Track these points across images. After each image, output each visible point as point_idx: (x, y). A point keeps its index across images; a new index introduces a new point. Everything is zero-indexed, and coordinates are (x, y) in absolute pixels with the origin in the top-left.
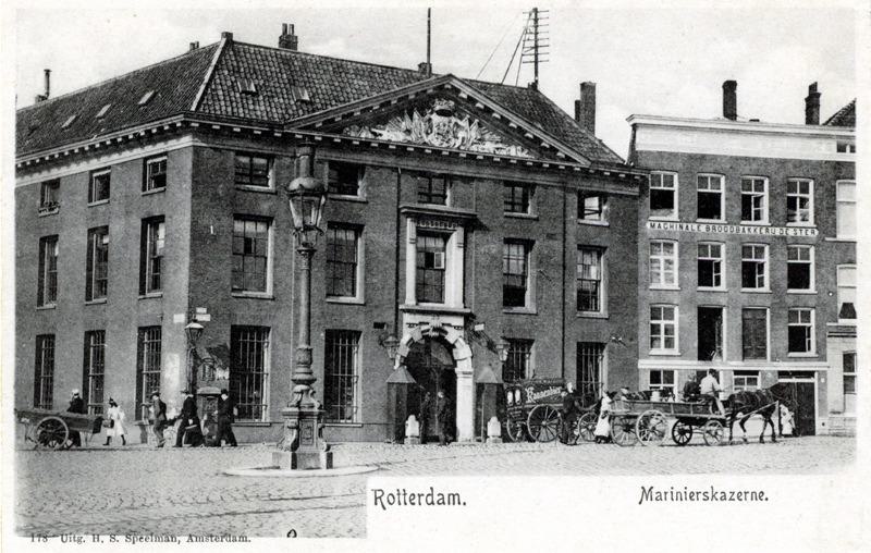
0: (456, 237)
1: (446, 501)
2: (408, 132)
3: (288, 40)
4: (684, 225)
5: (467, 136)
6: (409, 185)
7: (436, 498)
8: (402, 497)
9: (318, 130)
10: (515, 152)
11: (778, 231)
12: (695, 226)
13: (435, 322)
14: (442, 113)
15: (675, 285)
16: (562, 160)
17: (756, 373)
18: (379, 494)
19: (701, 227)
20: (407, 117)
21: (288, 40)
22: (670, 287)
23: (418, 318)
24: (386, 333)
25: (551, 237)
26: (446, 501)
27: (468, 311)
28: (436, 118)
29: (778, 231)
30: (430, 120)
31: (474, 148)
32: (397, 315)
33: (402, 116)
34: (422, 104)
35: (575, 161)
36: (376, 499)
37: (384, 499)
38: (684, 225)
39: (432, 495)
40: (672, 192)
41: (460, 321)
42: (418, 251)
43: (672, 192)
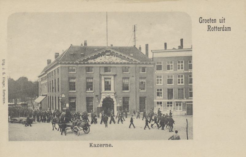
0: (113, 78)
1: (227, 30)
2: (101, 59)
3: (85, 44)
4: (164, 72)
5: (114, 59)
6: (103, 70)
7: (225, 29)
8: (215, 29)
9: (82, 61)
10: (124, 61)
11: (186, 72)
12: (166, 72)
13: (108, 95)
14: (107, 55)
15: (162, 84)
16: (134, 61)
17: (181, 102)
18: (209, 27)
19: (168, 72)
20: (101, 57)
21: (85, 44)
22: (161, 85)
23: (105, 94)
24: (98, 97)
25: (133, 77)
26: (227, 30)
27: (115, 92)
28: (107, 57)
29: (186, 72)
30: (105, 57)
31: (115, 61)
32: (100, 94)
33: (100, 56)
34: (103, 54)
35: (136, 61)
36: (208, 28)
37: (211, 29)
38: (164, 72)
39: (224, 28)
40: (161, 65)
41: (113, 94)
42: (105, 82)
43: (161, 65)
